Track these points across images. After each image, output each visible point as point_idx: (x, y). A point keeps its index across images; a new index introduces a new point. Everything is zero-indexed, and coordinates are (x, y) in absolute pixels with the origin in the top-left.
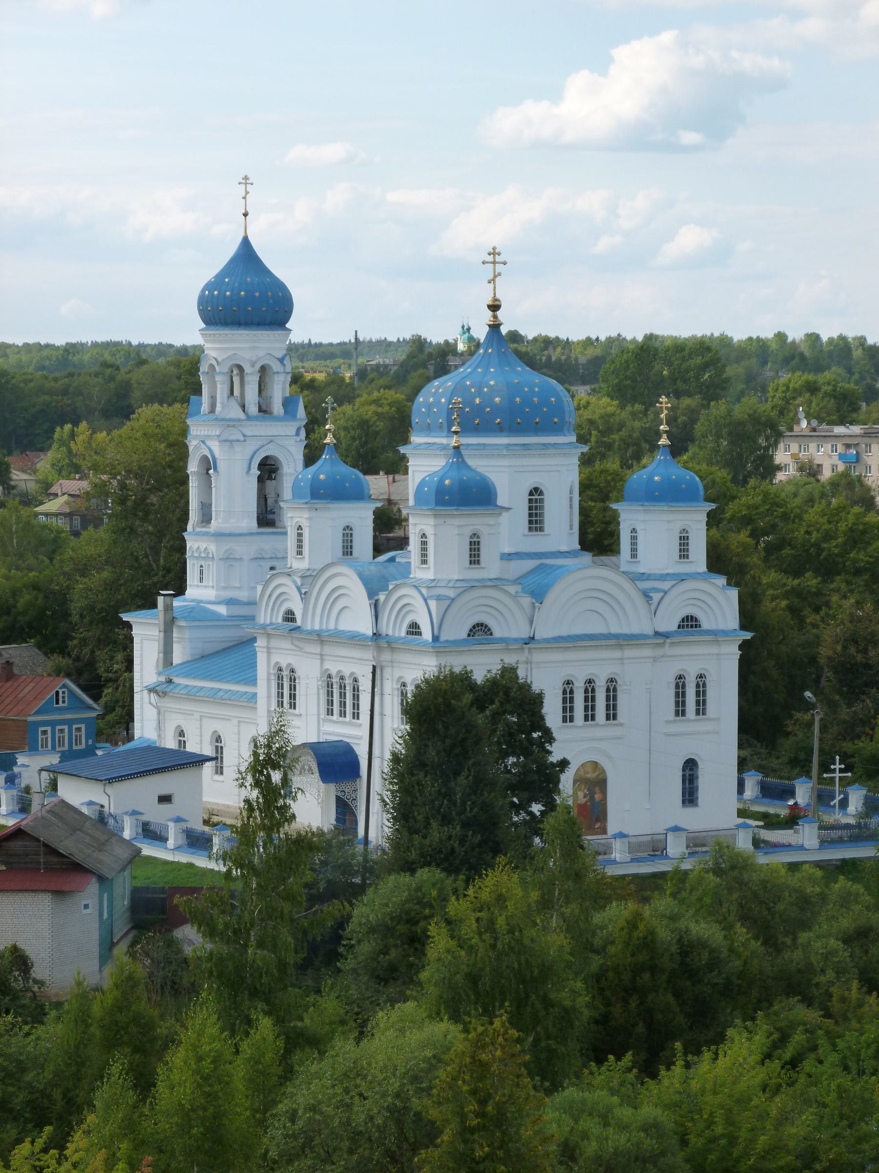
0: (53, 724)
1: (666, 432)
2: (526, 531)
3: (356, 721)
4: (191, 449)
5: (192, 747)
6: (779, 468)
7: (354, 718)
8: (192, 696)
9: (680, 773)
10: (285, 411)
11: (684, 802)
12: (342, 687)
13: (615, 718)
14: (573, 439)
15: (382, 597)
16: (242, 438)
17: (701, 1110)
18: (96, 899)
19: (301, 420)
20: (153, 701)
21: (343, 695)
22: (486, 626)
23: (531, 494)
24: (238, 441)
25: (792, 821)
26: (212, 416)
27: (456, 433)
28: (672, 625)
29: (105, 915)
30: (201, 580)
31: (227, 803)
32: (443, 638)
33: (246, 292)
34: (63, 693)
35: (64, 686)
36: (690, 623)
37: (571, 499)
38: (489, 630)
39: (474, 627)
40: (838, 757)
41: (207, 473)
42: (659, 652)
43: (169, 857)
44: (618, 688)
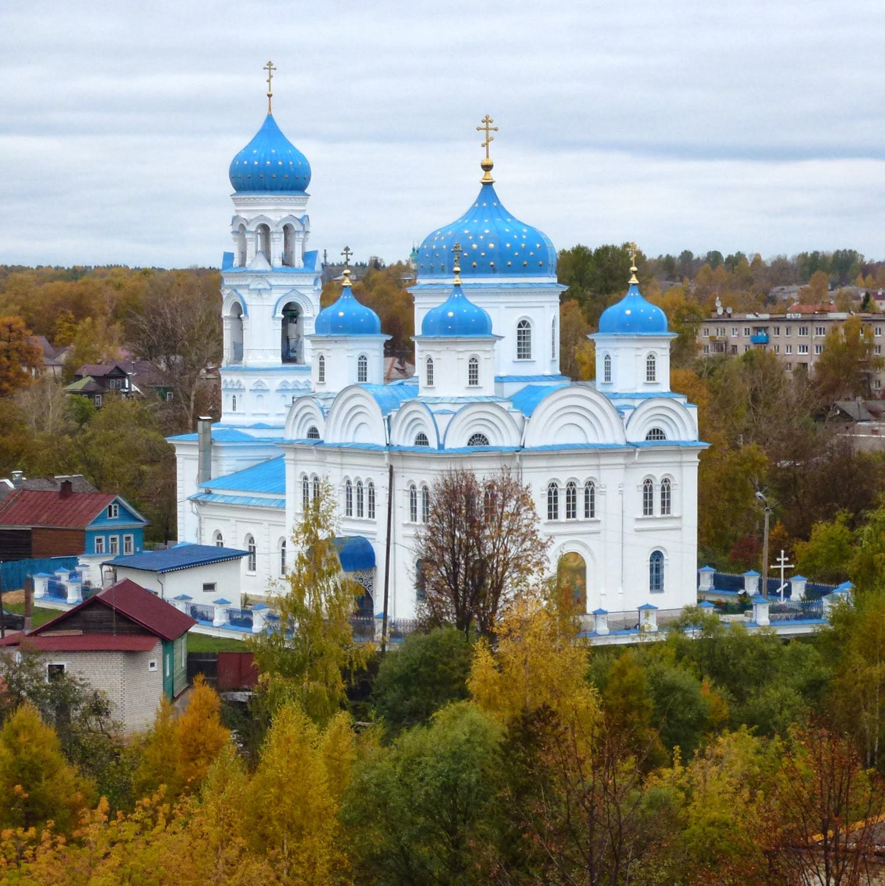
0: (106, 532)
1: (635, 272)
2: (516, 359)
3: (371, 519)
4: (224, 297)
5: (229, 543)
6: (699, 347)
7: (370, 517)
8: (228, 506)
9: (649, 563)
10: (305, 265)
11: (651, 588)
12: (360, 491)
13: (592, 515)
14: (555, 280)
15: (393, 414)
16: (268, 287)
17: (735, 741)
18: (161, 658)
19: (319, 272)
20: (195, 510)
21: (360, 498)
22: (483, 437)
23: (520, 326)
24: (265, 289)
25: (745, 606)
26: (242, 269)
27: (457, 272)
28: (638, 434)
29: (168, 674)
30: (234, 408)
31: (258, 594)
32: (447, 447)
33: (271, 161)
34: (115, 507)
35: (116, 501)
36: (656, 434)
37: (553, 331)
38: (486, 439)
39: (473, 437)
40: (783, 552)
41: (239, 318)
42: (630, 460)
43: (215, 634)
44: (595, 490)
